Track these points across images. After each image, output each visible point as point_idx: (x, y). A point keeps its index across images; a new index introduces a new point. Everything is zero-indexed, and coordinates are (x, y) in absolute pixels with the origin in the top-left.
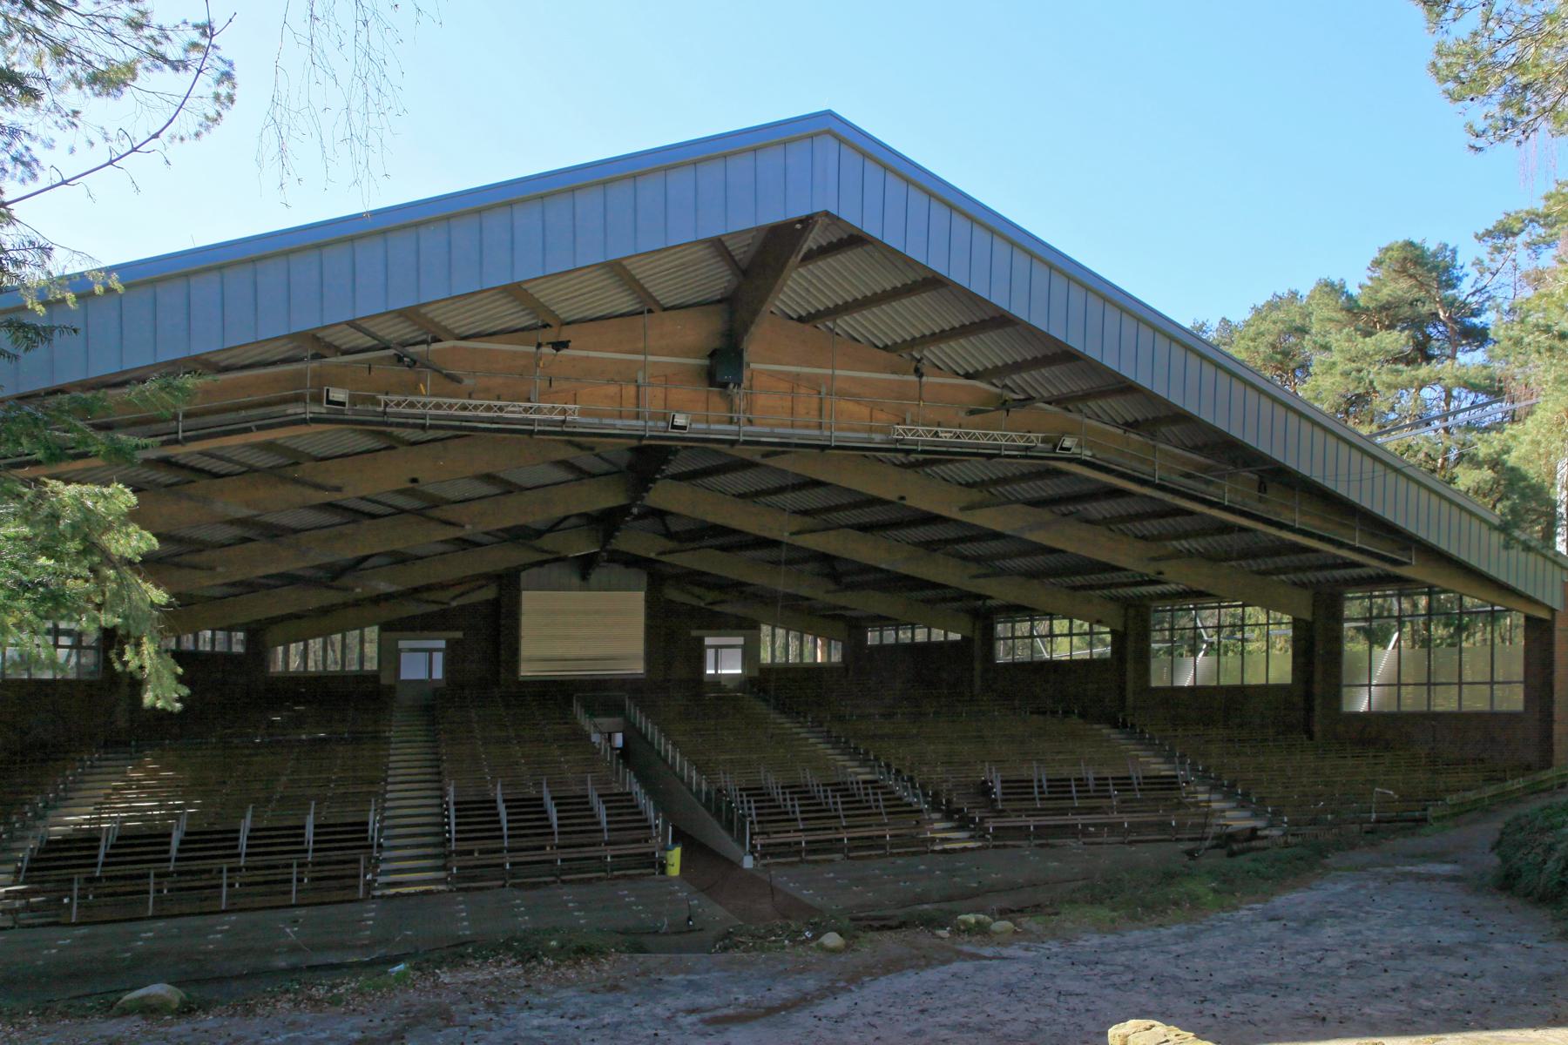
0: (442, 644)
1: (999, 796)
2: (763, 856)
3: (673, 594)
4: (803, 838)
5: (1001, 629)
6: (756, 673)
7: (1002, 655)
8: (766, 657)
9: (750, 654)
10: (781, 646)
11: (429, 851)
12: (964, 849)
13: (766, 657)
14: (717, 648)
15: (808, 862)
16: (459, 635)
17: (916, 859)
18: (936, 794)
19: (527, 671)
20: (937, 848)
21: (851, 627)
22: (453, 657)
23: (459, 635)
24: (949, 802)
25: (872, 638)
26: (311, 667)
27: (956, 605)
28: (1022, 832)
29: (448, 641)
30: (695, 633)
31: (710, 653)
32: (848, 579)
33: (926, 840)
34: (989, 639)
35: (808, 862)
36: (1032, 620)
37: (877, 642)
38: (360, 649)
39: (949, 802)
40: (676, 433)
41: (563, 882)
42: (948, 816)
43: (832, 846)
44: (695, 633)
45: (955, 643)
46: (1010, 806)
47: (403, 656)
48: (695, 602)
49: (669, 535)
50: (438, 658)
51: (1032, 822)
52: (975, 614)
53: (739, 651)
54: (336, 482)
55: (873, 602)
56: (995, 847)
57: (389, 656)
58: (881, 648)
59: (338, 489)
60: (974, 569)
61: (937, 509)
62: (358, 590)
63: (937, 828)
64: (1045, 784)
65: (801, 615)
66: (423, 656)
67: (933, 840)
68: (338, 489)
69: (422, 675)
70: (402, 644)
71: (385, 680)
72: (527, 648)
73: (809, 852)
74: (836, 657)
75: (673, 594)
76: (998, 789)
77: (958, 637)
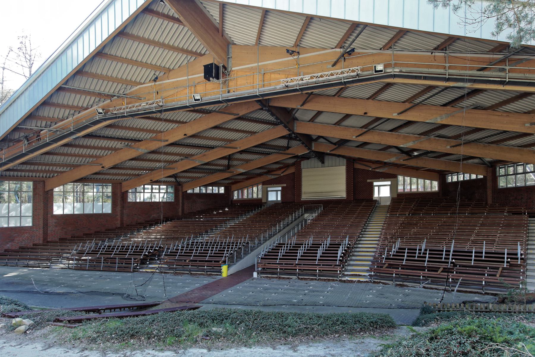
0: (280, 188)
4: (279, 267)
5: (27, 186)
6: (395, 196)
7: (502, 183)
8: (400, 188)
9: (393, 188)
10: (411, 185)
11: (357, 250)
14: (379, 186)
16: (285, 185)
21: (441, 176)
23: (285, 185)
25: (449, 179)
29: (282, 187)
30: (368, 181)
31: (376, 189)
34: (495, 178)
37: (468, 179)
38: (255, 192)
40: (197, 102)
44: (368, 181)
45: (481, 179)
47: (269, 193)
48: (367, 168)
50: (279, 193)
53: (389, 187)
54: (166, 139)
57: (266, 193)
59: (167, 141)
60: (454, 142)
61: (445, 122)
66: (274, 193)
68: (167, 141)
70: (269, 189)
71: (264, 201)
77: (482, 177)
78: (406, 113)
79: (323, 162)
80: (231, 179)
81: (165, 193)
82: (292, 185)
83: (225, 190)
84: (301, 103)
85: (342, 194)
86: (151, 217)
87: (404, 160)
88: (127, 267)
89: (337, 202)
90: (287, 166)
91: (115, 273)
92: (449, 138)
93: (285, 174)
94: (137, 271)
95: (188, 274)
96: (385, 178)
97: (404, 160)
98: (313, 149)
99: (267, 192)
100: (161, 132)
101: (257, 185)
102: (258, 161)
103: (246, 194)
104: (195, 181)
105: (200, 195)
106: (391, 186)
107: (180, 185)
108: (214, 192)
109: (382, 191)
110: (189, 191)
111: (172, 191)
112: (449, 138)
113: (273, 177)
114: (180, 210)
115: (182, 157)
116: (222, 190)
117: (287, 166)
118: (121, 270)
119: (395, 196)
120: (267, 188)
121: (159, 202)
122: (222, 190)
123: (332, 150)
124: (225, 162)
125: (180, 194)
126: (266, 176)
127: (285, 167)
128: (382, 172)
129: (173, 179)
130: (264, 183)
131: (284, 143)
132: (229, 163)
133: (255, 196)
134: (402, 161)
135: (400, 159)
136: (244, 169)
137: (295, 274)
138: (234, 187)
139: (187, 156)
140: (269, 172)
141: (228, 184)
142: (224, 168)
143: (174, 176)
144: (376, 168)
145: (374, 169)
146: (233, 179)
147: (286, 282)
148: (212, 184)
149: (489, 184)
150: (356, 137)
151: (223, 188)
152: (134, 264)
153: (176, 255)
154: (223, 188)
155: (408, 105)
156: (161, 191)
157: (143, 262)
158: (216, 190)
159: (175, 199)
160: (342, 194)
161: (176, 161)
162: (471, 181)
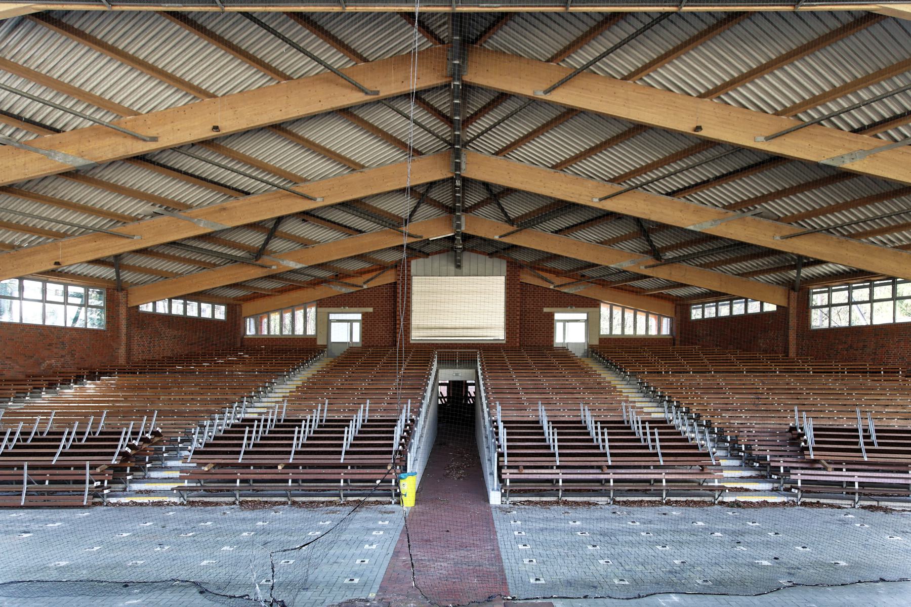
0: (359, 317)
1: (811, 444)
2: (513, 493)
3: (527, 278)
4: (561, 476)
5: (819, 299)
6: (596, 342)
7: (818, 320)
9: (592, 325)
12: (765, 504)
13: (604, 330)
15: (566, 503)
16: (371, 310)
17: (693, 512)
18: (735, 441)
19: (416, 335)
20: (728, 499)
22: (367, 324)
23: (371, 310)
24: (749, 448)
25: (696, 314)
26: (272, 333)
27: (771, 277)
28: (845, 489)
29: (365, 315)
30: (546, 310)
31: (559, 327)
32: (669, 255)
33: (712, 489)
34: (805, 308)
35: (566, 503)
36: (44, 282)
38: (301, 323)
39: (749, 448)
41: (294, 503)
42: (748, 462)
43: (597, 488)
44: (546, 310)
46: (824, 456)
48: (545, 285)
49: (510, 221)
50: (357, 327)
51: (857, 478)
52: (791, 286)
54: (152, 133)
55: (698, 279)
56: (804, 504)
57: (324, 325)
58: (703, 321)
59: (154, 139)
60: (787, 229)
62: (274, 267)
63: (729, 473)
64: (874, 436)
65: (627, 289)
67: (722, 489)
68: (154, 139)
69: (346, 339)
70: (332, 317)
71: (320, 342)
72: (416, 320)
73: (567, 492)
74: (666, 331)
75: (527, 278)
76: (809, 435)
78: (783, 137)
79: (458, 266)
80: (248, 288)
81: (81, 306)
82: (388, 310)
83: (228, 313)
84: (546, 86)
85: (498, 333)
86: (44, 366)
87: (646, 267)
88: (776, 456)
89: (488, 349)
90: (383, 268)
91: (22, 514)
92: (779, 219)
93: (372, 284)
94: (101, 504)
95: (284, 503)
96: (572, 305)
97: (646, 267)
98: (463, 229)
99: (329, 322)
100: (129, 112)
101: (304, 306)
102: (330, 246)
103: (276, 325)
104: (163, 283)
105: (169, 319)
106: (587, 321)
107: (122, 290)
108: (203, 315)
109: (570, 330)
110: (147, 308)
111: (100, 303)
112: (779, 219)
113: (345, 290)
114: (122, 351)
115: (157, 209)
116: (220, 313)
117: (383, 268)
118: (42, 501)
119: (596, 342)
120: (329, 313)
121: (64, 329)
122: (220, 313)
123: (505, 236)
124: (255, 239)
125: (123, 311)
126: (327, 285)
127: (376, 270)
128: (572, 295)
129: (109, 273)
130: (320, 304)
131: (401, 207)
132: (267, 242)
133: (299, 331)
134: (642, 267)
135: (639, 264)
136: (299, 261)
137: (606, 494)
138: (247, 307)
139: (173, 207)
140: (340, 277)
141: (235, 299)
142: (248, 255)
143: (115, 262)
144: (561, 286)
145: (558, 286)
146: (289, 280)
147: (583, 513)
148: (199, 297)
149: (793, 322)
150: (601, 200)
151: (223, 308)
152: (91, 482)
153: (239, 453)
154: (223, 308)
155: (787, 122)
156: (71, 300)
157: (117, 474)
158: (207, 311)
159: (108, 322)
160: (498, 333)
161: (136, 219)
162: (747, 318)
